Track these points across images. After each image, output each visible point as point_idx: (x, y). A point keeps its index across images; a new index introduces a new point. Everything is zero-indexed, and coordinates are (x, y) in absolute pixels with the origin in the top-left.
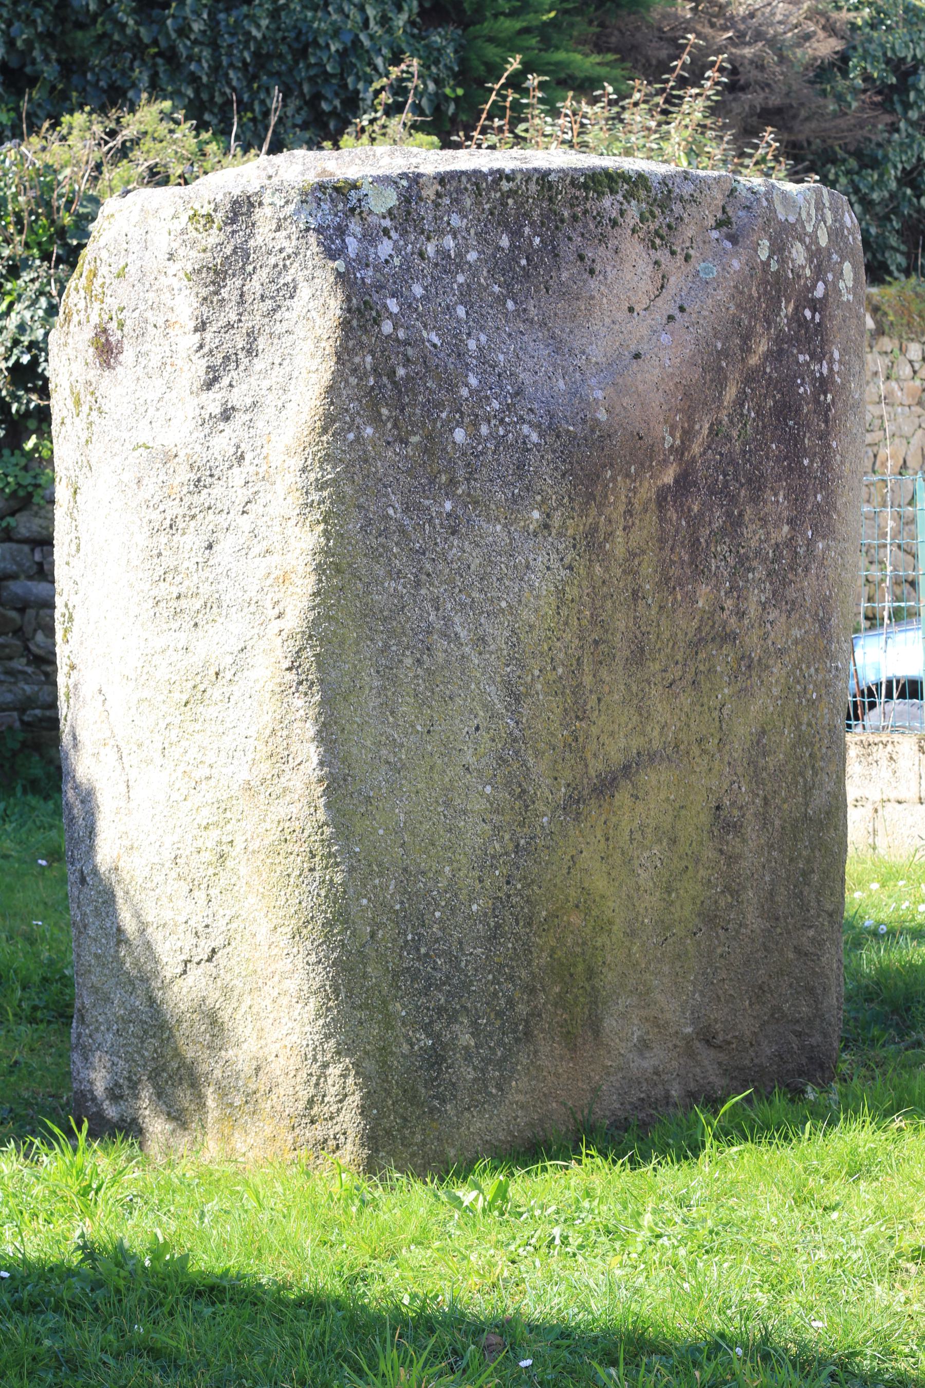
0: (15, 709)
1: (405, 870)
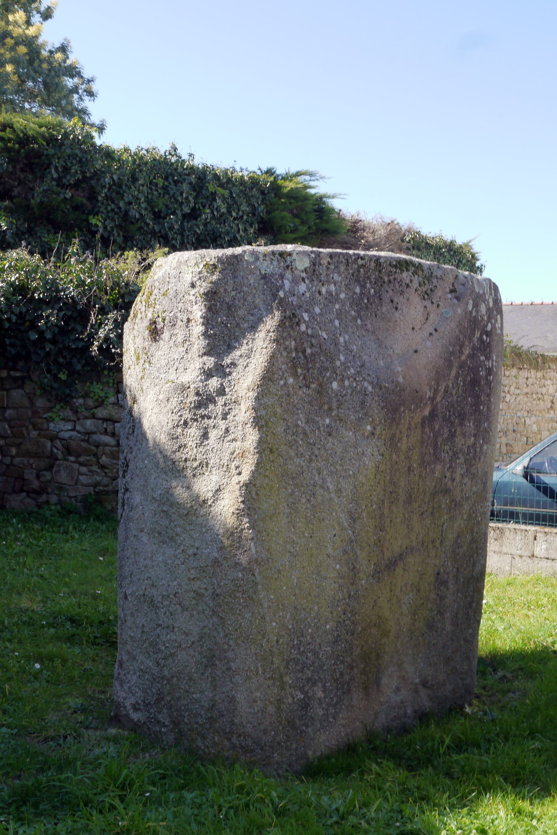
0: (92, 486)
1: (295, 608)
